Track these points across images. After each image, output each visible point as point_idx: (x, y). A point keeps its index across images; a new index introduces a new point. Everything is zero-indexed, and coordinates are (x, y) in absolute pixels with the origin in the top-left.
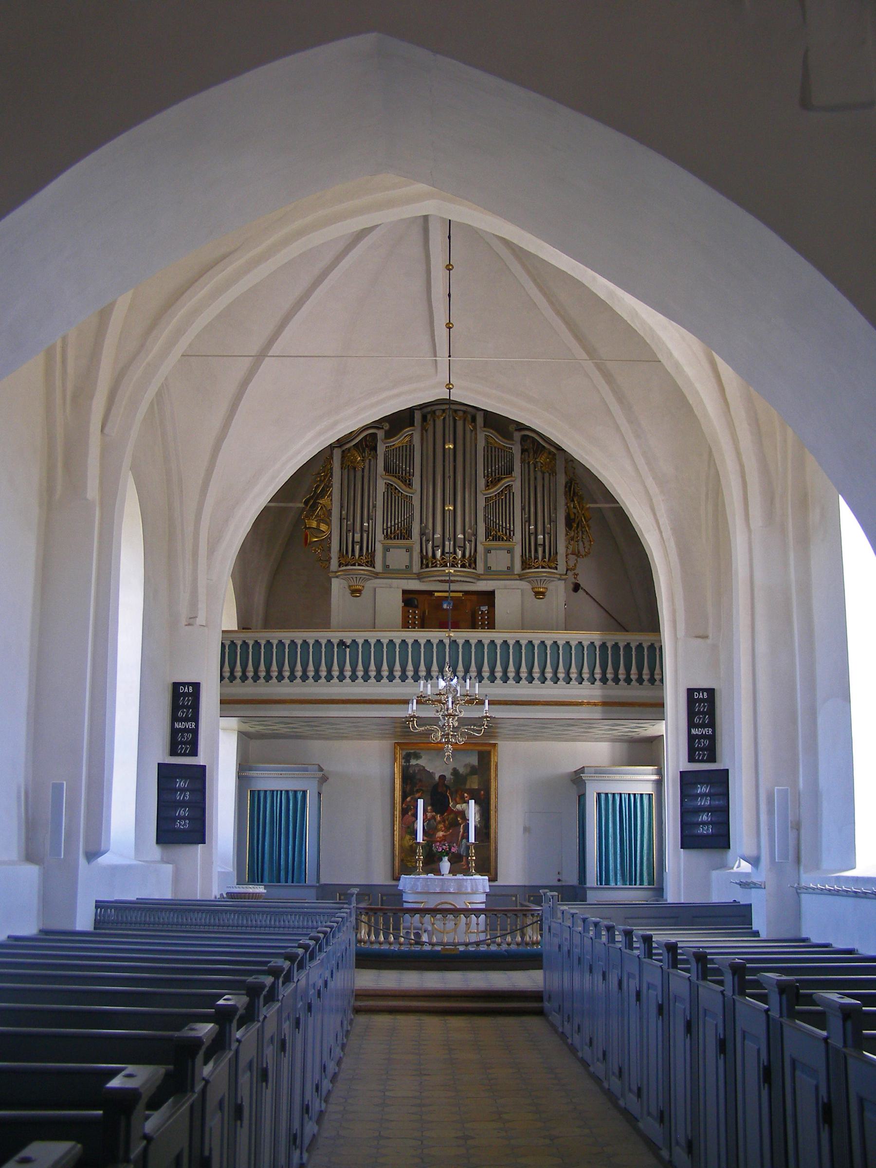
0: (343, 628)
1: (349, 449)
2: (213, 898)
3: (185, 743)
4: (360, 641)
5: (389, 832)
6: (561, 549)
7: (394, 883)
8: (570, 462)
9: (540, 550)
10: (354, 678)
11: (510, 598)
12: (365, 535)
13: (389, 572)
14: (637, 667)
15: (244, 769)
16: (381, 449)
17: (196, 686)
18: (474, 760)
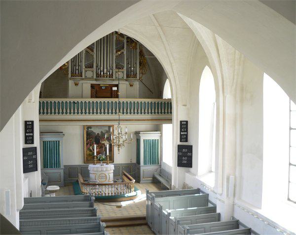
0: (72, 98)
3: (30, 140)
4: (80, 102)
6: (138, 72)
8: (141, 45)
9: (132, 72)
10: (63, 113)
11: (124, 87)
13: (86, 78)
17: (32, 122)
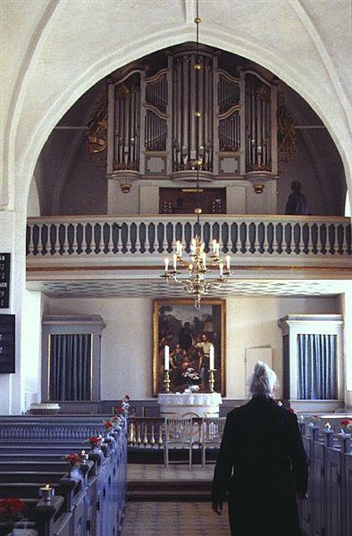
0: (117, 214)
1: (120, 85)
2: (21, 414)
4: (129, 224)
5: (149, 364)
7: (155, 399)
10: (143, 250)
11: (237, 191)
12: (132, 148)
13: (149, 175)
14: (339, 242)
15: (47, 317)
16: (144, 85)
18: (209, 311)
